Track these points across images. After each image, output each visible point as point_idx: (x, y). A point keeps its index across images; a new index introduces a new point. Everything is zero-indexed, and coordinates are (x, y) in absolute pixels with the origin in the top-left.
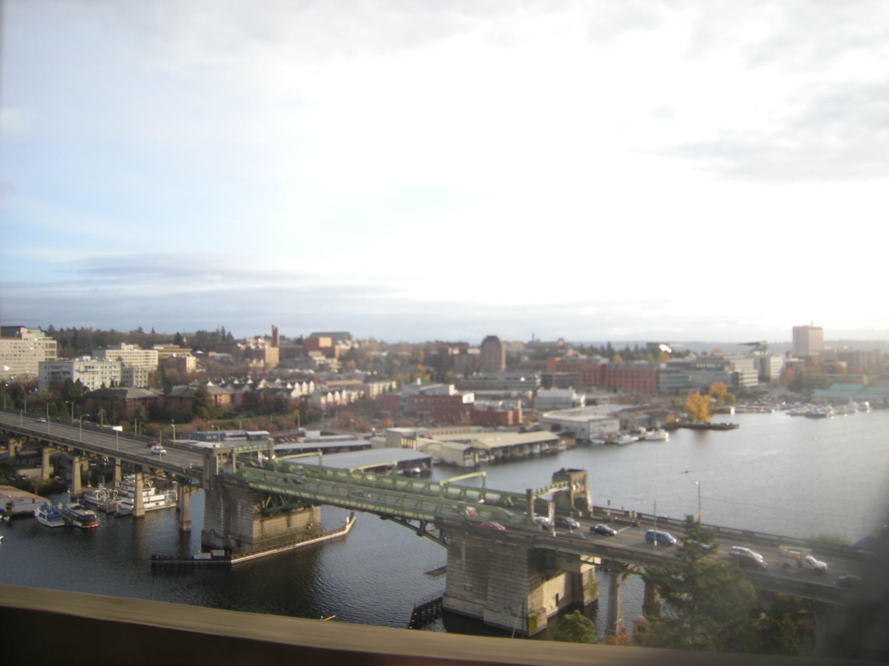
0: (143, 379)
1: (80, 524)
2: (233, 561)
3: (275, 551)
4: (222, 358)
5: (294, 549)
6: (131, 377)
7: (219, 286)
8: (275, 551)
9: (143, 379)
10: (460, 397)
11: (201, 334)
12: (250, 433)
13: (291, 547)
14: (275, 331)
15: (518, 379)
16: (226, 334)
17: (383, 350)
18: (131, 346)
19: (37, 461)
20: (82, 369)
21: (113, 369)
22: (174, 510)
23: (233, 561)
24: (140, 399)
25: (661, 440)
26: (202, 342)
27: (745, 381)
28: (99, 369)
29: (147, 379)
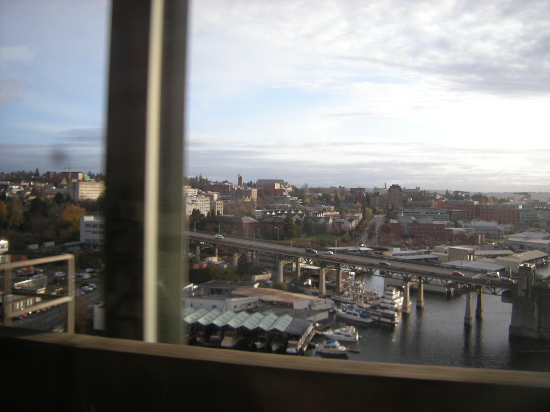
14: (240, 179)
15: (437, 213)
20: (191, 202)
21: (206, 202)
24: (249, 224)
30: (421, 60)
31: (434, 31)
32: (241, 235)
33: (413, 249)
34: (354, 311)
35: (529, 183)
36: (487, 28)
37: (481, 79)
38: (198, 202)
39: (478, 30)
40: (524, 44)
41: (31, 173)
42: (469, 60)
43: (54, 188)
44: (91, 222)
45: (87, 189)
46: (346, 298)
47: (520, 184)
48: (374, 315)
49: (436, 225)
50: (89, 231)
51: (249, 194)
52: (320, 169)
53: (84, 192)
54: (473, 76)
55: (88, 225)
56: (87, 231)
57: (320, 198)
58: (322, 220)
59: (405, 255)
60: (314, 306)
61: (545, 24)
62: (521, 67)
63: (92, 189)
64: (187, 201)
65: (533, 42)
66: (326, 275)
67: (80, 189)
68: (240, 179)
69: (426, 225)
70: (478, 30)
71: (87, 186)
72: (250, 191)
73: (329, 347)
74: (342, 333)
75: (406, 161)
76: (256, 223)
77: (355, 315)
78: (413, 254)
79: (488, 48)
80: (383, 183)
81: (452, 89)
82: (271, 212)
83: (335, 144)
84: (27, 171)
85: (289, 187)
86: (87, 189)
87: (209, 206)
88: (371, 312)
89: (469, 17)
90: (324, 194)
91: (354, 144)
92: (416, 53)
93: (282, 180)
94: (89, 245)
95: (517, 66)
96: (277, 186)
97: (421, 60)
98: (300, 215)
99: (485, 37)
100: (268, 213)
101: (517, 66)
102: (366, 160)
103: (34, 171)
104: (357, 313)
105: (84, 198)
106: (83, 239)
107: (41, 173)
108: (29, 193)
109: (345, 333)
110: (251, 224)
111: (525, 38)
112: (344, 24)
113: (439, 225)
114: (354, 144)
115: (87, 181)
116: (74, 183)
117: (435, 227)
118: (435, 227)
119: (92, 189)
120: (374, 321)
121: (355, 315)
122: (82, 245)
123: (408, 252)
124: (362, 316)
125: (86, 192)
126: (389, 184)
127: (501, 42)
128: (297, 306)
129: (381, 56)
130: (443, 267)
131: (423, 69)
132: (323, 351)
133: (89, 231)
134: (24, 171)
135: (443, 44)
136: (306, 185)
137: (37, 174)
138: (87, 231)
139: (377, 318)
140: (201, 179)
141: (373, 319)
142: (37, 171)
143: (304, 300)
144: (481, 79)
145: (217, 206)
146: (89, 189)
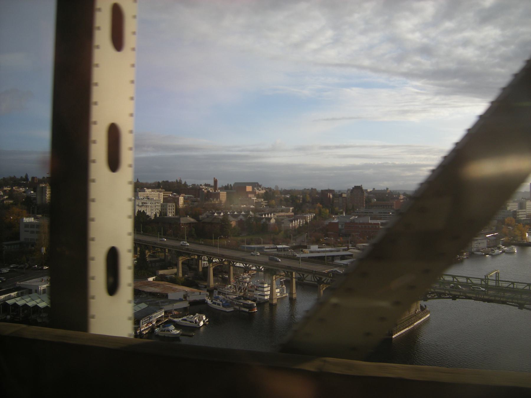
0: (173, 210)
1: (247, 310)
2: (16, 293)
3: (407, 329)
4: (188, 197)
5: (413, 328)
6: (166, 209)
7: (194, 153)
8: (407, 329)
9: (173, 210)
10: (179, 219)
11: (179, 183)
12: (278, 246)
13: (412, 327)
14: (216, 182)
15: (389, 213)
16: (183, 183)
17: (287, 194)
18: (150, 190)
19: (173, 264)
20: (140, 204)
21: (157, 204)
22: (288, 299)
23: (394, 337)
24: (187, 224)
25: (512, 253)
26: (268, 188)
27: (520, 216)
28: (149, 204)
29: (174, 211)
30: (406, 66)
31: (416, 38)
32: (178, 236)
33: (335, 247)
34: (218, 302)
36: (467, 34)
37: (464, 83)
39: (459, 36)
40: (503, 49)
41: (22, 179)
42: (452, 66)
43: (32, 192)
44: (31, 222)
46: (227, 291)
48: (237, 305)
49: (371, 224)
50: (28, 231)
51: (217, 196)
54: (456, 81)
55: (27, 225)
56: (26, 231)
57: (286, 200)
58: (264, 220)
59: (324, 252)
60: (189, 296)
61: (522, 29)
62: (503, 71)
65: (513, 47)
66: (214, 270)
68: (216, 182)
69: (363, 224)
70: (459, 36)
72: (219, 194)
73: (164, 331)
74: (188, 319)
75: (397, 163)
76: (195, 223)
77: (219, 304)
78: (331, 251)
79: (469, 53)
80: (344, 186)
81: (437, 93)
82: (265, 215)
83: (327, 148)
84: (18, 177)
85: (263, 189)
87: (160, 208)
88: (235, 303)
89: (448, 25)
91: (345, 147)
92: (400, 59)
93: (257, 183)
95: (498, 70)
97: (406, 66)
98: (243, 215)
99: (466, 43)
100: (216, 214)
101: (498, 70)
104: (221, 303)
106: (22, 239)
108: (6, 197)
109: (190, 320)
110: (190, 224)
111: (504, 43)
112: (330, 33)
113: (374, 224)
114: (345, 147)
115: (157, 186)
116: (42, 187)
117: (370, 226)
118: (370, 226)
120: (236, 311)
121: (219, 304)
123: (327, 249)
124: (223, 306)
126: (351, 186)
128: (171, 296)
129: (367, 62)
130: (298, 259)
131: (410, 75)
132: (160, 334)
133: (28, 231)
135: (425, 50)
137: (26, 179)
138: (26, 231)
139: (237, 307)
140: (180, 182)
141: (235, 309)
142: (27, 176)
143: (180, 291)
144: (464, 83)
145: (168, 208)
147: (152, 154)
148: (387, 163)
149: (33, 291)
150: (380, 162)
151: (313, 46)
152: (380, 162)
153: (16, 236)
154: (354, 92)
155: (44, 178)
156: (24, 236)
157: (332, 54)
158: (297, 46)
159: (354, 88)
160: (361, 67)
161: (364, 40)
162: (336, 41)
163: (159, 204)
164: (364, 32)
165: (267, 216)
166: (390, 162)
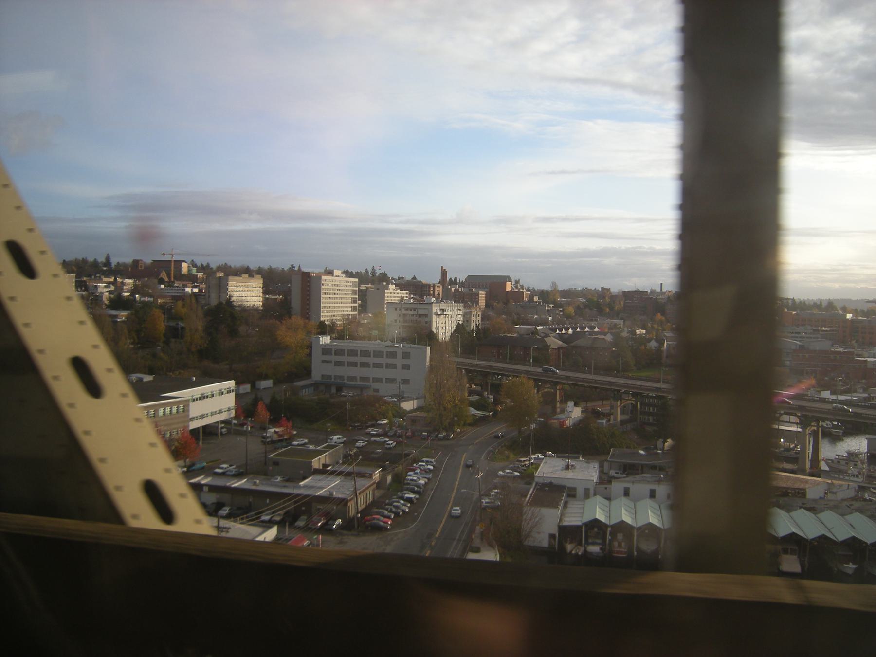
14: (444, 273)
35: (852, 285)
38: (448, 312)
45: (238, 289)
47: (837, 286)
52: (519, 260)
53: (235, 294)
56: (324, 361)
63: (246, 289)
64: (434, 311)
67: (230, 288)
68: (444, 273)
71: (238, 284)
82: (561, 330)
83: (547, 220)
86: (238, 289)
90: (589, 300)
91: (577, 219)
94: (328, 386)
96: (509, 287)
102: (594, 245)
103: (102, 259)
105: (245, 303)
107: (114, 261)
111: (865, 50)
112: (573, 25)
114: (577, 219)
119: (246, 289)
122: (316, 385)
125: (238, 294)
127: (826, 56)
129: (629, 77)
134: (554, 284)
136: (554, 284)
137: (108, 263)
138: (324, 361)
143: (818, 483)
146: (241, 289)
147: (254, 226)
148: (640, 247)
149: (580, 492)
150: (624, 245)
151: (542, 46)
152: (629, 246)
153: (306, 371)
154: (599, 127)
155: (136, 262)
156: (319, 370)
157: (572, 62)
158: (516, 45)
159: (599, 121)
160: (619, 85)
161: (629, 37)
162: (582, 39)
163: (479, 313)
164: (630, 25)
165: (564, 332)
166: (646, 245)
